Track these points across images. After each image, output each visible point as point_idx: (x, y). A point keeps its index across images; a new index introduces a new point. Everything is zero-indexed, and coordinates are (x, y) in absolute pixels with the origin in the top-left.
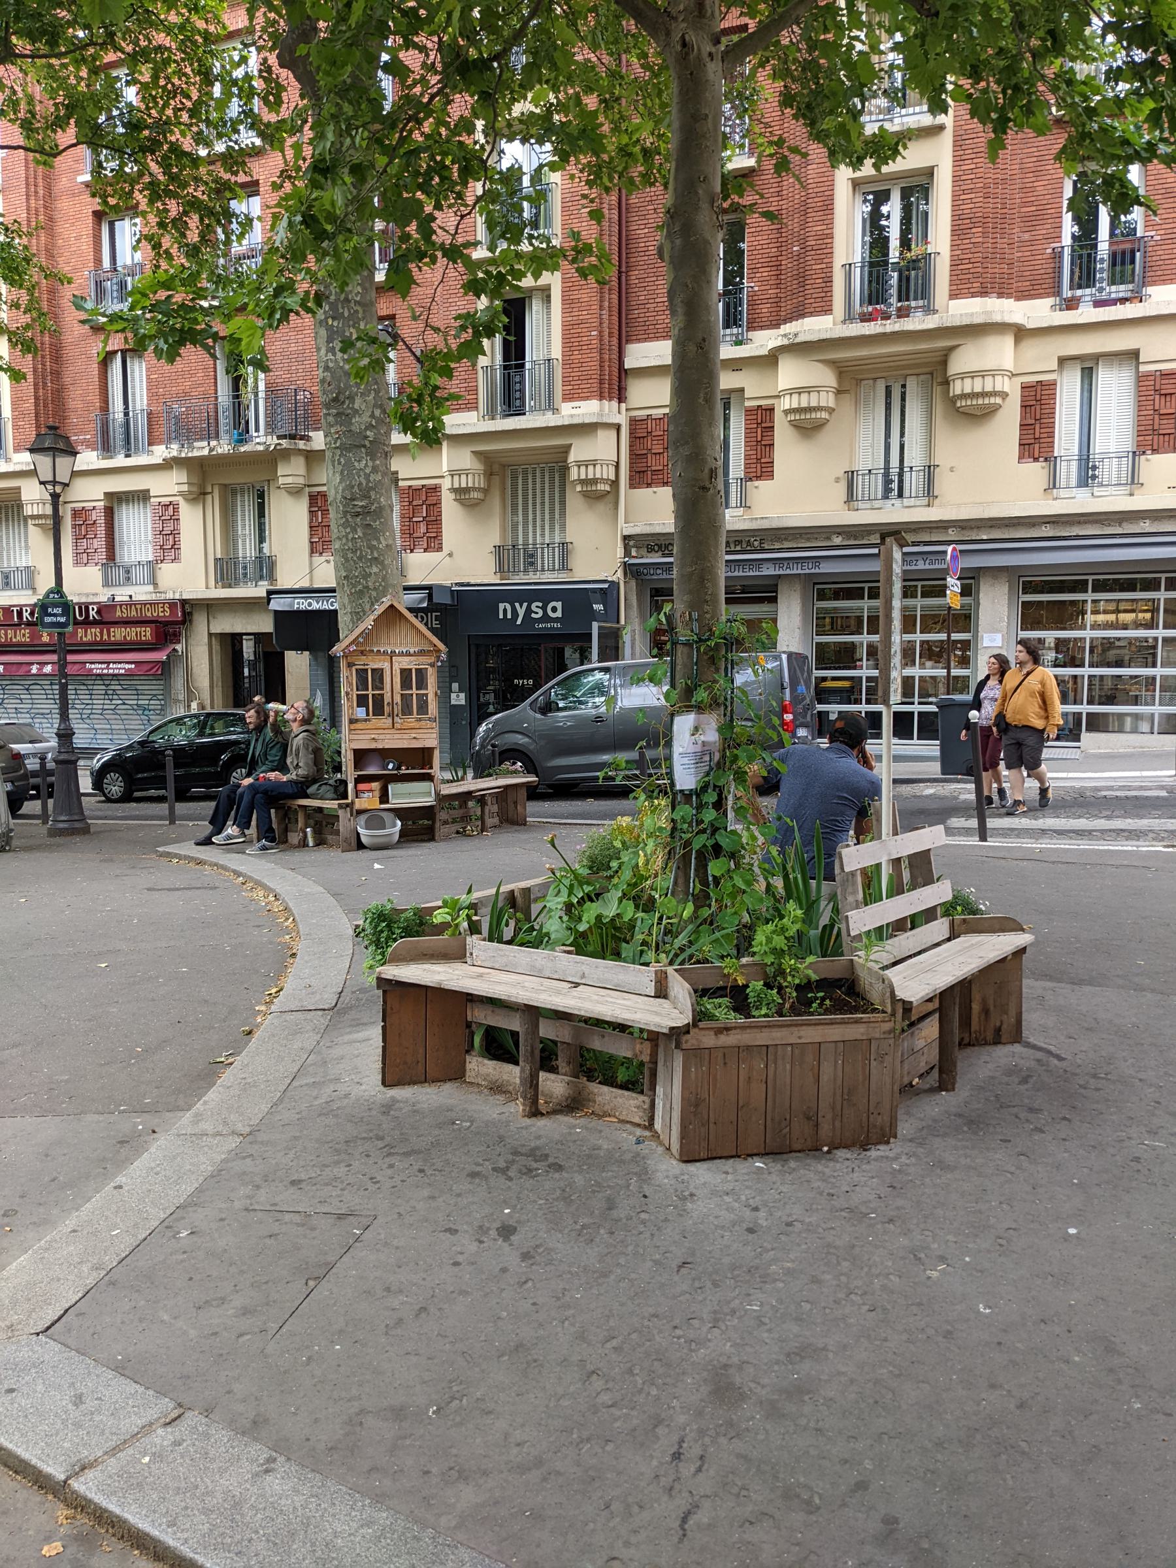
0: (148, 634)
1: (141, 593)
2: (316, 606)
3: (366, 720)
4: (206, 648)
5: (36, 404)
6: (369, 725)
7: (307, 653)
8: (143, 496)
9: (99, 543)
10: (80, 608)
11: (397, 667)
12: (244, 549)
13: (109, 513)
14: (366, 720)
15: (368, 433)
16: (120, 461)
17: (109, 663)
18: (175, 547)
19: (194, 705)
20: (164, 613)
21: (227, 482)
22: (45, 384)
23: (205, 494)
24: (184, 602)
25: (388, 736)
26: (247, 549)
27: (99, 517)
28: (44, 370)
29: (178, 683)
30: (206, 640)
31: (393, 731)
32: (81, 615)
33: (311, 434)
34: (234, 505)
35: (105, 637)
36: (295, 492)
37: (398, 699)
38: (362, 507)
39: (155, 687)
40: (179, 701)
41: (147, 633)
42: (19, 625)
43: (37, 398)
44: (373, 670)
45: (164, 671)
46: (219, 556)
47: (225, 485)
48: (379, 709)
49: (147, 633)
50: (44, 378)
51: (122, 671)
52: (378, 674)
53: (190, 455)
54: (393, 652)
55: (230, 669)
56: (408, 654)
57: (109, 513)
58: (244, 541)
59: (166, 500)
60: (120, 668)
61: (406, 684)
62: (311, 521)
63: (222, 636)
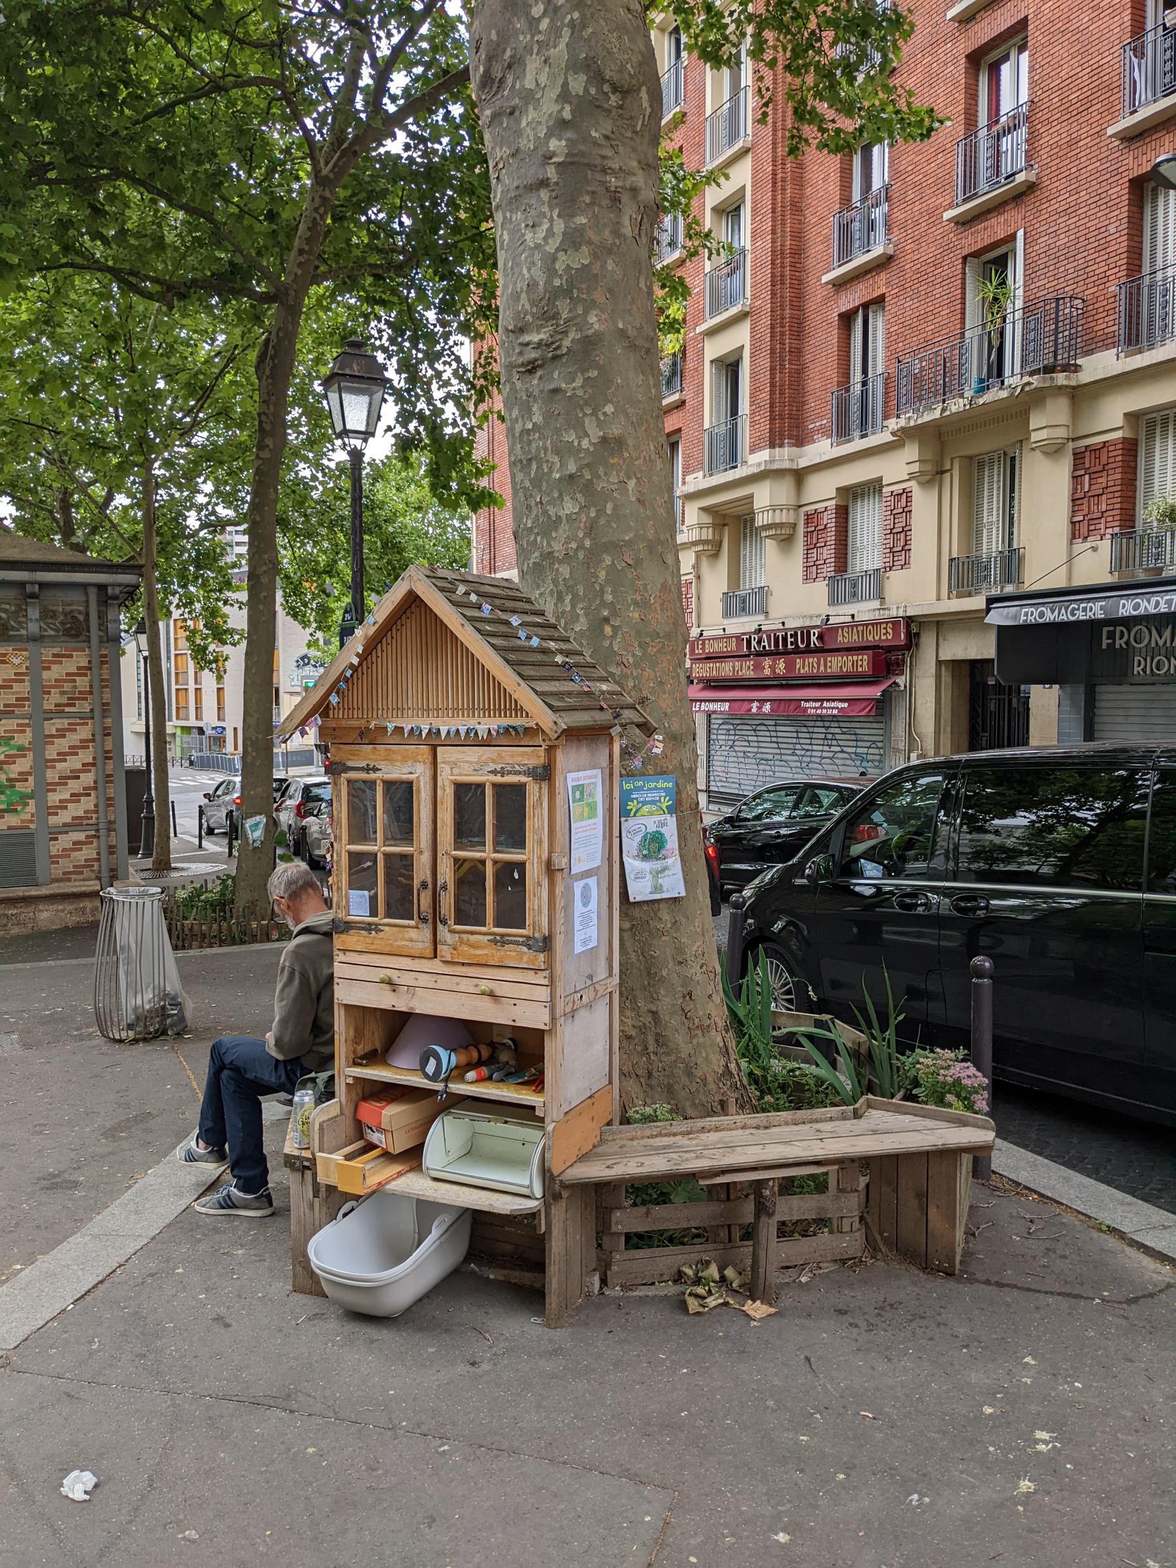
0: (865, 663)
1: (865, 610)
2: (1050, 617)
3: (369, 928)
4: (932, 680)
5: (772, 393)
6: (377, 940)
7: (1057, 686)
8: (873, 487)
9: (828, 553)
10: (802, 633)
11: (446, 777)
12: (990, 542)
13: (843, 513)
14: (369, 928)
15: (554, 144)
16: (857, 445)
17: (822, 701)
18: (906, 549)
19: (913, 756)
20: (885, 636)
21: (968, 452)
22: (782, 366)
23: (943, 472)
24: (909, 620)
25: (424, 980)
26: (992, 544)
27: (829, 519)
28: (783, 349)
29: (899, 727)
30: (933, 670)
31: (436, 966)
32: (802, 642)
33: (1079, 362)
34: (981, 480)
35: (822, 668)
36: (1053, 451)
37: (446, 873)
38: (539, 344)
39: (869, 731)
40: (899, 751)
41: (862, 663)
42: (748, 656)
43: (772, 385)
44: (389, 784)
45: (882, 708)
46: (955, 555)
47: (971, 458)
48: (400, 903)
49: (862, 663)
50: (782, 359)
51: (835, 712)
52: (402, 796)
53: (919, 421)
54: (434, 733)
55: (965, 709)
56: (473, 740)
57: (843, 513)
58: (990, 531)
59: (897, 488)
60: (832, 709)
61: (467, 829)
62: (1075, 490)
63: (956, 665)
